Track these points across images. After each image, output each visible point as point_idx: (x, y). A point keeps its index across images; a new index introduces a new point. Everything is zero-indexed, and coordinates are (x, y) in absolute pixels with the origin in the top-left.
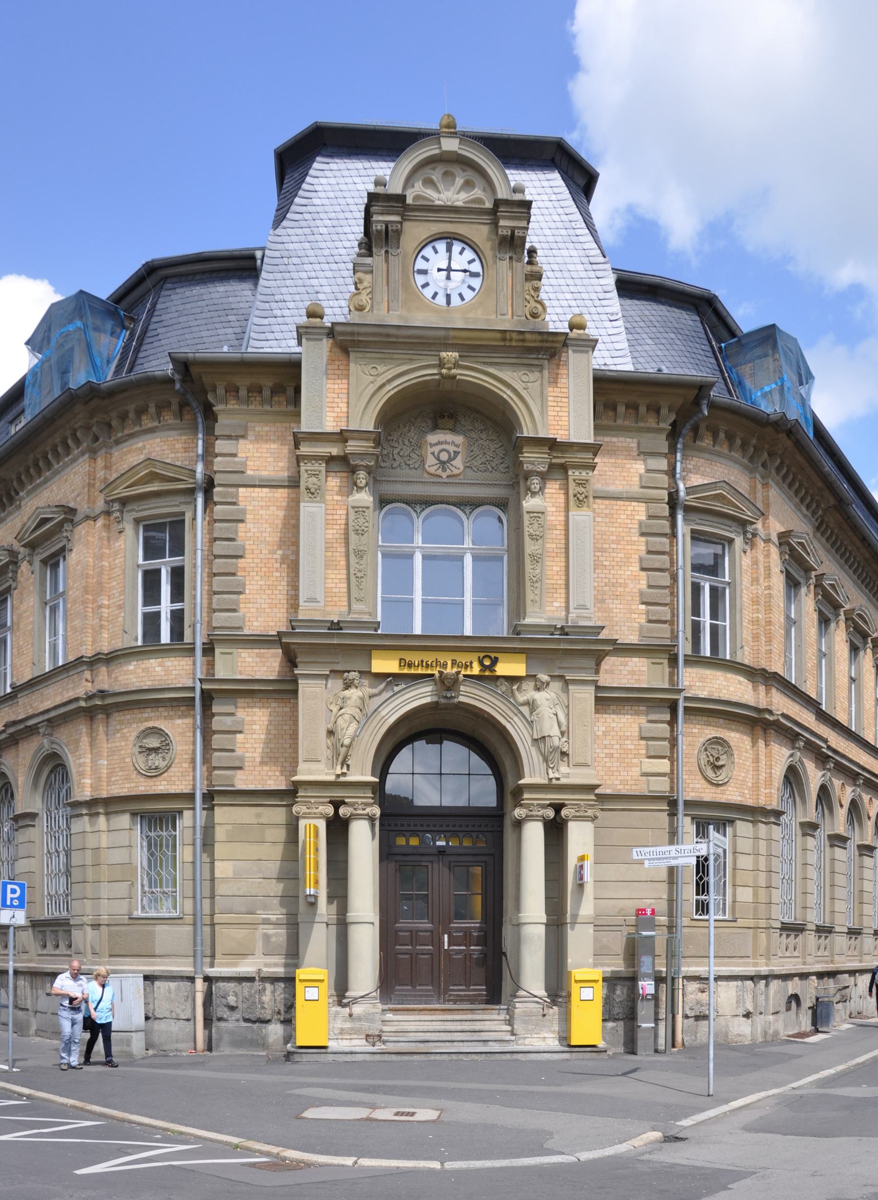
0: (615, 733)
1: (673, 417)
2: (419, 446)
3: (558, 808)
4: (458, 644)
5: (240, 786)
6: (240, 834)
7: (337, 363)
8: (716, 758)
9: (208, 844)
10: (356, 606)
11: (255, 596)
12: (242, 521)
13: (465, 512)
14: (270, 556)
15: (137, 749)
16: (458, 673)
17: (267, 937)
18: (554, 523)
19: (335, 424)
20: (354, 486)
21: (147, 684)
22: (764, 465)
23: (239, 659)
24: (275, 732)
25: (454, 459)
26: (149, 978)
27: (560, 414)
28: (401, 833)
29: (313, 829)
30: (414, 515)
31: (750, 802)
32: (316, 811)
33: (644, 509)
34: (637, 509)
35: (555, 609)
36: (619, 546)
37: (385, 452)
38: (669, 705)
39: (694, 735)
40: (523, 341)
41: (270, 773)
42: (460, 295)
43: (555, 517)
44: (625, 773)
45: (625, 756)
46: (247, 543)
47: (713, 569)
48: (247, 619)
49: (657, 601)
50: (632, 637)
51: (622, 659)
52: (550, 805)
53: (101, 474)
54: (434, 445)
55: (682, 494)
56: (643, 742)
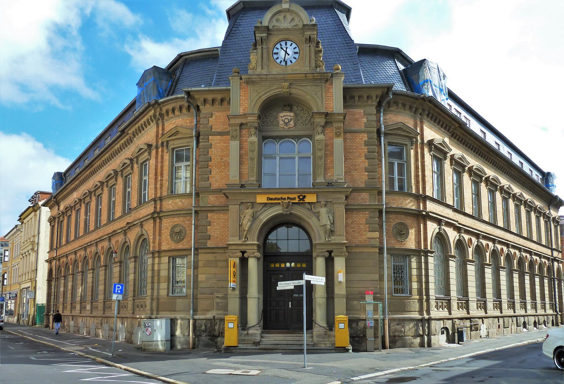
3: (330, 252)
4: (291, 190)
5: (209, 246)
6: (208, 264)
22: (420, 114)
28: (272, 262)
42: (291, 61)
47: (399, 155)
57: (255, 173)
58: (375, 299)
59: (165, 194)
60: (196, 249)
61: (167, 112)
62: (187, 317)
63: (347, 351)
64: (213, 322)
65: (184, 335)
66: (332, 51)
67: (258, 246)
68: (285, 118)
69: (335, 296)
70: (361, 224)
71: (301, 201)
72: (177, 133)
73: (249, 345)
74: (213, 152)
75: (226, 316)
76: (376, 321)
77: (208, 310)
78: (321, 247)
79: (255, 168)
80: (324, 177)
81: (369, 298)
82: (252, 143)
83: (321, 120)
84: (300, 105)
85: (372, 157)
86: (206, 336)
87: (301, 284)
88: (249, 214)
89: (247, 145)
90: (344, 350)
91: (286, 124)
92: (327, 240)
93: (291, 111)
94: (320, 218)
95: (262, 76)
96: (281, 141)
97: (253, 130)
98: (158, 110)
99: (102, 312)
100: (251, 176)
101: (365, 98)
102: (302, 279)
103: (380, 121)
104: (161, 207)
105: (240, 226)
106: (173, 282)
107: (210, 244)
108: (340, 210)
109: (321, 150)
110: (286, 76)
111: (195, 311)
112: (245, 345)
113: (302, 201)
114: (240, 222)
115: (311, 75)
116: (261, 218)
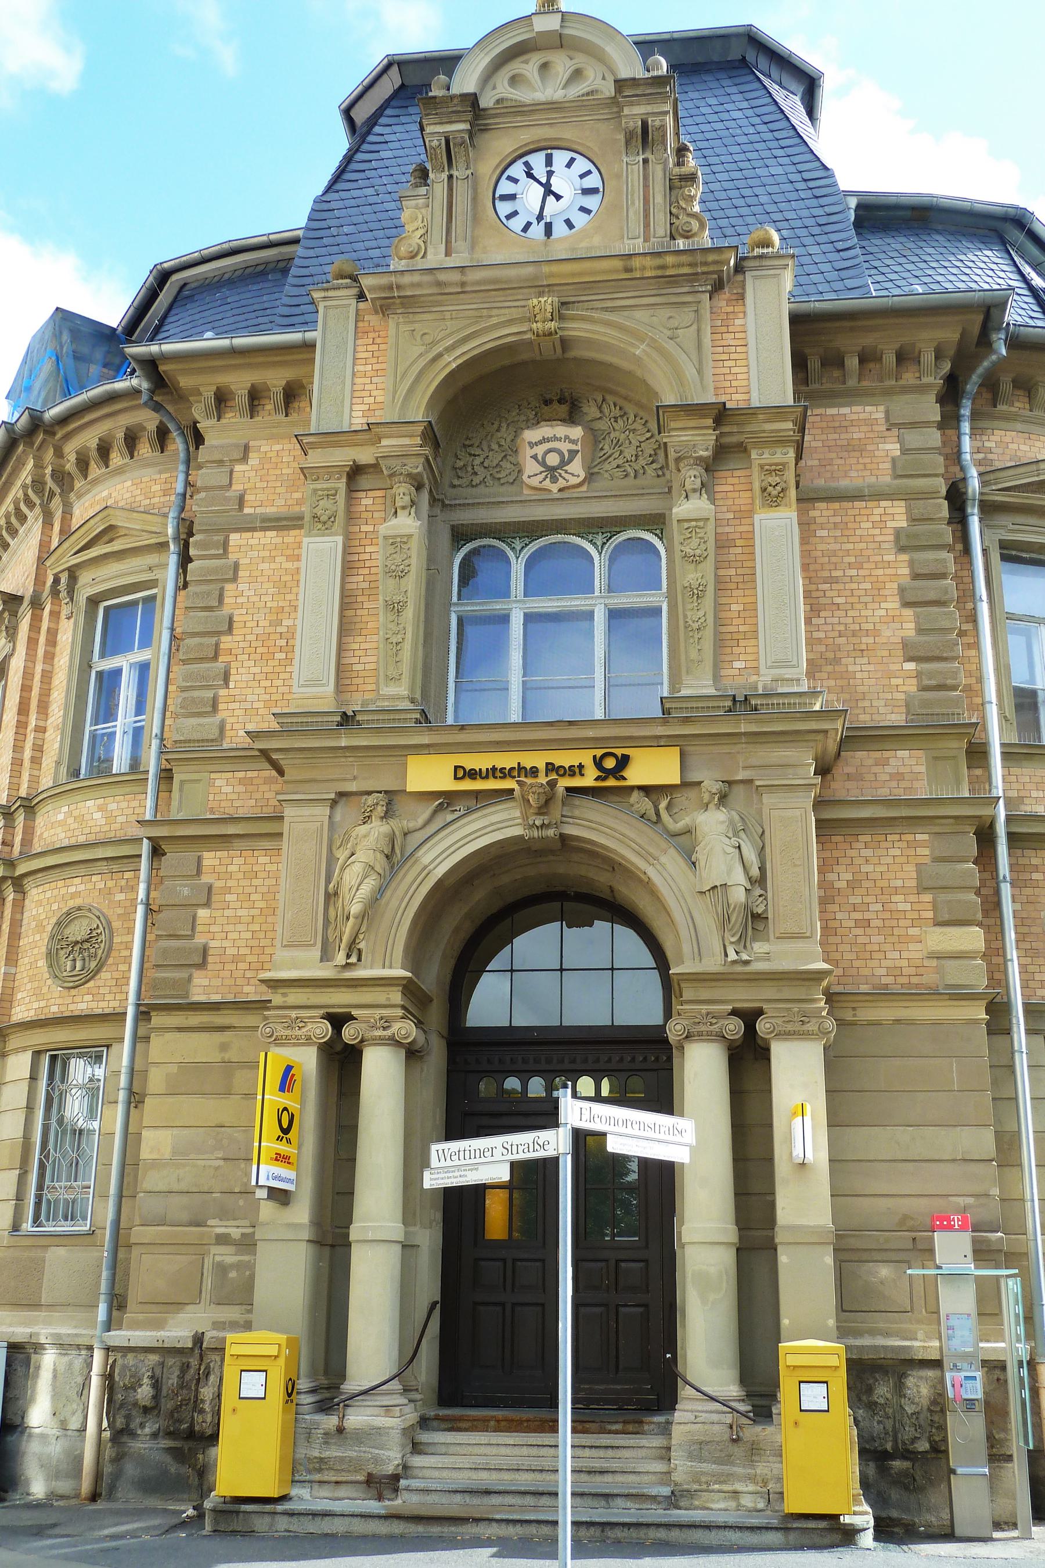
0: (870, 884)
3: (750, 1017)
4: (566, 732)
6: (191, 1080)
7: (371, 335)
11: (244, 691)
13: (594, 544)
14: (271, 630)
16: (552, 784)
18: (731, 537)
19: (364, 420)
23: (211, 790)
24: (262, 904)
25: (570, 461)
27: (734, 370)
30: (511, 555)
32: (299, 1033)
33: (903, 510)
34: (889, 511)
35: (737, 672)
36: (861, 572)
37: (460, 464)
40: (663, 267)
41: (248, 974)
44: (896, 955)
45: (894, 923)
46: (236, 612)
48: (228, 727)
49: (937, 653)
50: (893, 717)
51: (878, 754)
52: (734, 1012)
54: (536, 444)
57: (405, 668)
58: (982, 1253)
59: (46, 781)
60: (143, 1014)
61: (83, 464)
62: (85, 1334)
63: (847, 1536)
64: (194, 1362)
65: (63, 1425)
66: (744, 211)
67: (409, 988)
68: (546, 453)
69: (780, 1237)
70: (896, 891)
71: (611, 782)
72: (109, 532)
73: (342, 1492)
74: (242, 598)
75: (231, 1337)
76: (995, 1368)
77: (176, 1305)
78: (705, 994)
79: (407, 646)
80: (717, 677)
81: (953, 1250)
82: (398, 542)
83: (700, 440)
84: (610, 399)
85: (932, 596)
86: (155, 1435)
87: (550, 1152)
88: (371, 841)
89: (375, 555)
90: (835, 1533)
91: (552, 472)
92: (732, 956)
93: (571, 418)
94: (700, 855)
95: (442, 277)
97: (403, 491)
98: (49, 455)
100: (391, 679)
101: (890, 359)
102: (556, 1125)
103: (959, 453)
104: (27, 842)
105: (331, 897)
106: (42, 1167)
107: (203, 987)
108: (793, 820)
109: (696, 560)
110: (546, 269)
111: (118, 1303)
112: (325, 1492)
113: (611, 785)
114: (328, 881)
115: (648, 262)
116: (426, 860)
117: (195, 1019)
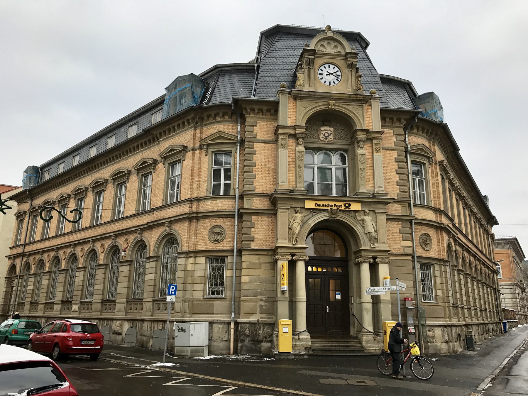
1: (405, 122)
2: (318, 130)
3: (375, 258)
5: (253, 247)
6: (252, 266)
8: (425, 242)
9: (239, 268)
10: (299, 185)
12: (255, 154)
15: (210, 233)
17: (261, 306)
20: (298, 144)
21: (216, 209)
22: (433, 138)
26: (211, 323)
29: (283, 264)
31: (437, 257)
38: (409, 221)
39: (419, 231)
43: (369, 156)
52: (372, 258)
53: (198, 135)
55: (409, 148)
56: (401, 235)
86: (249, 341)
91: (326, 137)
95: (310, 93)
96: (319, 153)
99: (124, 314)
107: (253, 246)
114: (289, 225)
115: (354, 96)
117: (252, 253)
